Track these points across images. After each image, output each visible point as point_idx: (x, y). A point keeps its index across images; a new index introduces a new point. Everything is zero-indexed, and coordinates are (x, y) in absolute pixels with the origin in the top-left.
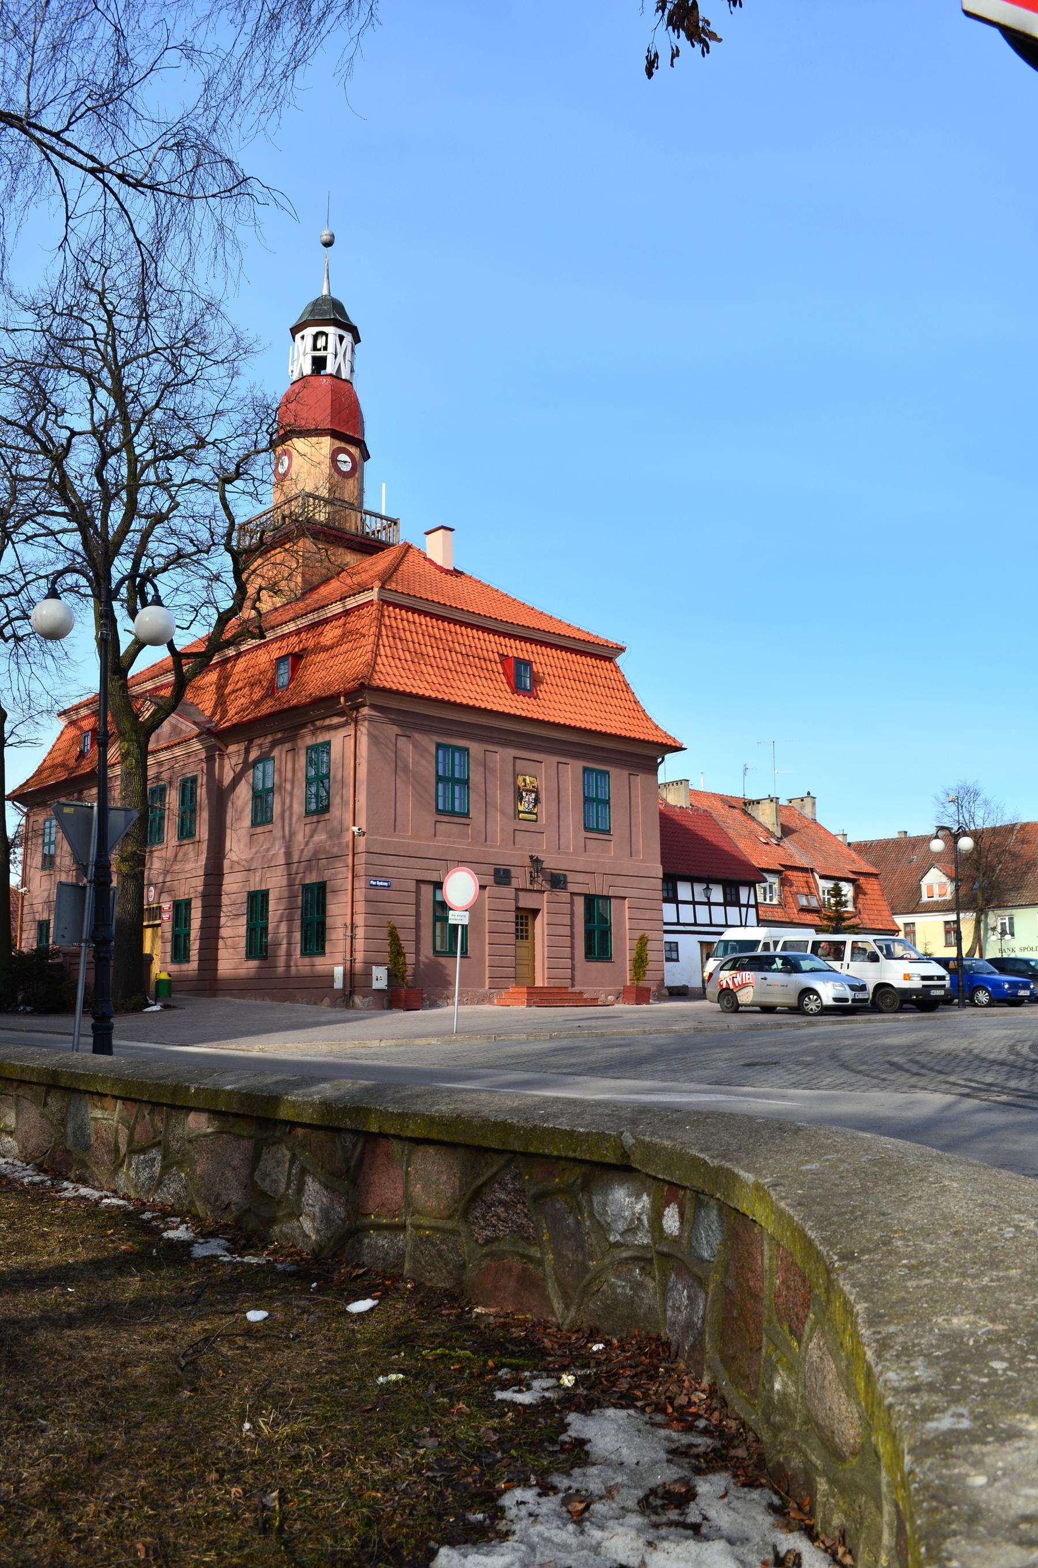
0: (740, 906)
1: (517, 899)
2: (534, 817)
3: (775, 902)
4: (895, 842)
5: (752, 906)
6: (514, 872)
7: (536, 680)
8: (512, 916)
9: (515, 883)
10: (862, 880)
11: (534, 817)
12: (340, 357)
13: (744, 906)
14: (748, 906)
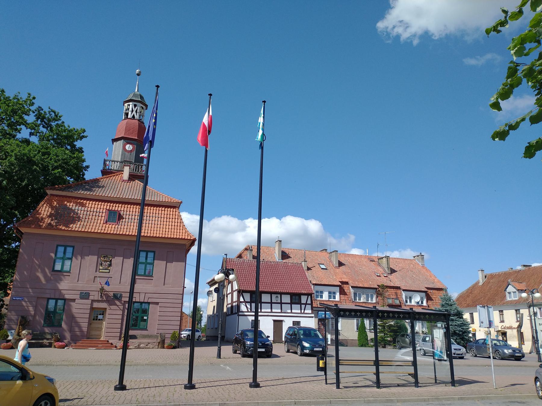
1: (92, 304)
6: (91, 293)
8: (88, 311)
9: (91, 298)
12: (134, 112)
14: (306, 304)
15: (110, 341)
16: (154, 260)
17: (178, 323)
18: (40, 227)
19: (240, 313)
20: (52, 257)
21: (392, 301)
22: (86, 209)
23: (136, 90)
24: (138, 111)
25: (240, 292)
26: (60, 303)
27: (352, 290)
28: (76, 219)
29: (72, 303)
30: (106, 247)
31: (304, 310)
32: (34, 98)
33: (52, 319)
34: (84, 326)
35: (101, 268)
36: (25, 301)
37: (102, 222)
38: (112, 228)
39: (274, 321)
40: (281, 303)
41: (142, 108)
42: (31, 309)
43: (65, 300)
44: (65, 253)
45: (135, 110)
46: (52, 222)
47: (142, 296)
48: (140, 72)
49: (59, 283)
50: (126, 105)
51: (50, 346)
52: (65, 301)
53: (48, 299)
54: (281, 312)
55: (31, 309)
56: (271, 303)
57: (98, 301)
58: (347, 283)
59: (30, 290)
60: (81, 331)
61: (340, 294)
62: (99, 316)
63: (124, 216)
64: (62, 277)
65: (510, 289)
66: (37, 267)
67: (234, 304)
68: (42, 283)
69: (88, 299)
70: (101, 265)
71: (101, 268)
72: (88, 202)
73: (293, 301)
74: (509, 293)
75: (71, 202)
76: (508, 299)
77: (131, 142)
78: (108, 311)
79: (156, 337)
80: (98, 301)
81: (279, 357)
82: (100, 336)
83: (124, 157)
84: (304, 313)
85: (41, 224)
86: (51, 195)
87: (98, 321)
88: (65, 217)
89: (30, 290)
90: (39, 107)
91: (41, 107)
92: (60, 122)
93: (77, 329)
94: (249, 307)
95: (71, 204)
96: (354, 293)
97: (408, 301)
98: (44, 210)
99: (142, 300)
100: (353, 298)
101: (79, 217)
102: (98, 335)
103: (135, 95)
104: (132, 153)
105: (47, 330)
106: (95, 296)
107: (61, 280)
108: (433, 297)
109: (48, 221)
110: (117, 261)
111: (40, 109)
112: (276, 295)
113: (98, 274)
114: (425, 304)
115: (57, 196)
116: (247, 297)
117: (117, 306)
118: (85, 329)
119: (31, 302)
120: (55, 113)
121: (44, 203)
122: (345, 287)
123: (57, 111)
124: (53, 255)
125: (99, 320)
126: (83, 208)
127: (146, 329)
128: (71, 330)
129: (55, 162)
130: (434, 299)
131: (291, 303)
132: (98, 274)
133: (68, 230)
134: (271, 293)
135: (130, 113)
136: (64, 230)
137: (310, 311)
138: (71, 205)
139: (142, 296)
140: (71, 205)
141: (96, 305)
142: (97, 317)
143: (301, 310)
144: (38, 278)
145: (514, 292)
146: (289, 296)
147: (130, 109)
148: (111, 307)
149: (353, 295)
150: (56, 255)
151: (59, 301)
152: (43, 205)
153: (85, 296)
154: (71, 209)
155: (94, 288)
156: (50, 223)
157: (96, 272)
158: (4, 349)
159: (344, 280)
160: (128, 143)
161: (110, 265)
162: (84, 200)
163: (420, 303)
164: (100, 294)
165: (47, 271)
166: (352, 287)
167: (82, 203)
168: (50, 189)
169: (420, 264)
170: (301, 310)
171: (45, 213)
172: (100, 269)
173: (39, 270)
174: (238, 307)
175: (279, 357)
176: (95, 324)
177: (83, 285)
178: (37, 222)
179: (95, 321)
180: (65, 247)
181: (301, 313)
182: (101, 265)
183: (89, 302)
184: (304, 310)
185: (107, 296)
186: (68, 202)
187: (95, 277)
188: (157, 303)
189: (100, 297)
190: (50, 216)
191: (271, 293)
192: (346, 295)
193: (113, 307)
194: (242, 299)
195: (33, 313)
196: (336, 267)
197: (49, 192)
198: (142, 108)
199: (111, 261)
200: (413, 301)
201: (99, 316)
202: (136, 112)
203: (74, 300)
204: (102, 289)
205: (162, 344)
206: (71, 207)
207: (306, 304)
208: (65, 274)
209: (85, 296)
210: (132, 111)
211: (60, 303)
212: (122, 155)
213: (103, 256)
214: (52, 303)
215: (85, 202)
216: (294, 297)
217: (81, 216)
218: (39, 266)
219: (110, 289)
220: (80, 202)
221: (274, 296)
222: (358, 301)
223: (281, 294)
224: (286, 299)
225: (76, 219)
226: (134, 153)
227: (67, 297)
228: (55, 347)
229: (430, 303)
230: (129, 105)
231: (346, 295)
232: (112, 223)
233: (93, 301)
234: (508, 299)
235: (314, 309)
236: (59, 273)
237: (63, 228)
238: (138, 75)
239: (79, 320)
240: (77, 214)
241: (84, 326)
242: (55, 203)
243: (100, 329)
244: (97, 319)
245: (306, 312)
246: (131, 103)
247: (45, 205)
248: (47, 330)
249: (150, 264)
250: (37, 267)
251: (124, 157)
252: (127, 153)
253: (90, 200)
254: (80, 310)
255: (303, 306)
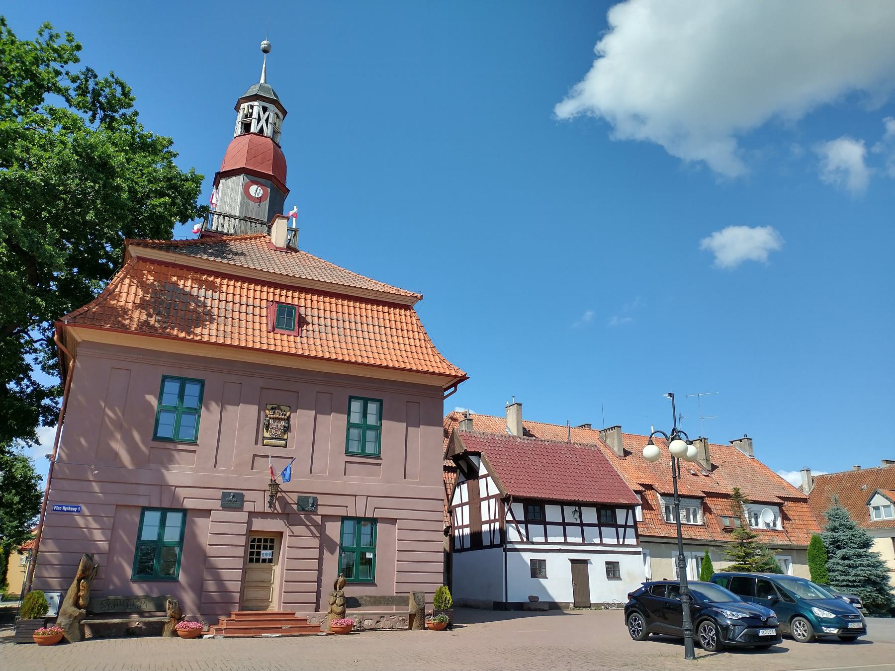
0: (617, 526)
1: (249, 523)
2: (283, 442)
3: (699, 522)
4: (850, 475)
5: (630, 527)
6: (248, 495)
7: (302, 322)
8: (242, 540)
9: (248, 507)
10: (708, 501)
11: (283, 442)
12: (263, 122)
13: (621, 526)
14: (625, 526)
15: (299, 615)
16: (380, 419)
17: (314, 575)
18: (125, 329)
19: (509, 546)
20: (149, 404)
21: (731, 522)
22: (223, 297)
23: (262, 81)
24: (270, 120)
25: (504, 500)
26: (174, 519)
27: (662, 501)
28: (203, 317)
29: (200, 521)
30: (284, 386)
31: (624, 538)
32: (78, 48)
33: (152, 561)
34: (232, 578)
35: (267, 435)
36: (84, 516)
37: (264, 328)
38: (285, 342)
39: (607, 563)
40: (582, 525)
41: (278, 116)
42: (98, 535)
43: (185, 512)
44: (181, 396)
45: (264, 117)
46: (152, 321)
47: (361, 502)
48: (269, 45)
49: (167, 469)
50: (245, 106)
51: (155, 630)
52: (185, 516)
53: (145, 509)
54: (583, 544)
55: (98, 535)
56: (564, 524)
57: (263, 515)
58: (649, 487)
59: (96, 487)
60: (223, 590)
61: (643, 509)
62: (263, 552)
63: (309, 319)
64: (175, 453)
65: (878, 500)
66: (112, 428)
67: (485, 528)
68: (125, 467)
69: (240, 509)
70: (267, 427)
71: (267, 435)
72: (225, 281)
73: (603, 520)
74: (877, 508)
75: (187, 279)
76: (874, 518)
77: (259, 180)
78: (286, 541)
79: (401, 601)
80: (263, 515)
81: (872, 643)
82: (267, 601)
83: (247, 210)
84: (624, 545)
85: (127, 322)
86: (140, 258)
87: (260, 565)
88: (176, 311)
89: (96, 487)
90: (88, 70)
91: (92, 71)
92: (129, 112)
93: (211, 586)
94: (523, 531)
95: (189, 283)
96: (667, 508)
97: (753, 520)
98: (126, 292)
99: (361, 514)
100: (664, 514)
101: (210, 313)
102: (262, 600)
103: (262, 87)
104: (263, 203)
105: (138, 590)
106: (257, 502)
107: (171, 460)
108: (790, 513)
109: (138, 316)
110: (301, 418)
111: (90, 73)
112: (573, 508)
113: (261, 450)
114: (779, 527)
115: (152, 262)
116: (519, 510)
117: (307, 526)
118: (234, 586)
119: (96, 517)
120: (123, 88)
121: (125, 277)
122: (649, 494)
123: (129, 85)
124: (153, 400)
125: (264, 561)
126: (217, 295)
127: (372, 583)
128: (199, 589)
129: (150, 182)
130: (791, 517)
131: (600, 525)
132: (261, 450)
133: (192, 341)
134: (562, 503)
135: (254, 123)
136: (184, 339)
137: (633, 541)
138: (187, 285)
139: (361, 502)
140: (187, 285)
141: (259, 525)
142: (259, 554)
143: (618, 538)
144: (116, 455)
145: (884, 507)
146: (594, 510)
147: (255, 115)
148: (293, 528)
149: (663, 510)
150: (160, 403)
151: (170, 515)
152: (123, 279)
153: (233, 501)
154: (190, 294)
155: (254, 482)
156: (146, 323)
157: (256, 443)
158: (41, 644)
159: (647, 482)
160: (254, 183)
161: (287, 429)
162: (217, 277)
163: (772, 525)
164: (268, 499)
165: (136, 436)
166: (663, 495)
167: (214, 282)
168: (138, 245)
169: (747, 454)
170: (618, 538)
171: (131, 298)
172: (264, 438)
173: (118, 436)
174: (503, 533)
175: (872, 643)
176: (257, 572)
177: (230, 476)
178: (114, 318)
179: (254, 565)
180: (183, 382)
181: (618, 545)
182: (267, 427)
183: (243, 516)
184: (624, 538)
185: (285, 504)
186: (180, 278)
187: (255, 456)
188: (393, 521)
189: (267, 505)
190: (143, 305)
191: (562, 503)
192: (653, 509)
193: (299, 530)
194: (509, 517)
195: (104, 545)
196: (620, 457)
197: (134, 251)
198: (278, 116)
199: (289, 418)
200: (760, 520)
201: (263, 552)
202: (267, 120)
203: (206, 513)
204: (274, 485)
205: (417, 620)
206: (188, 289)
207: (625, 526)
208: (180, 447)
209: (233, 501)
210: (259, 120)
211: (174, 519)
212: (242, 205)
213: (269, 407)
214: (152, 518)
215: (218, 280)
216: (603, 512)
217: (215, 311)
218: (119, 427)
219: (298, 484)
220: (206, 280)
221: (568, 510)
222: (692, 523)
223: (579, 504)
224: (590, 515)
225: (203, 317)
226: (266, 204)
227: (188, 504)
228: (175, 634)
229: (788, 524)
230: (252, 107)
231: (653, 509)
232: (283, 331)
233: (252, 515)
234: (874, 518)
235: (641, 539)
236: (170, 446)
237: (183, 335)
238: (265, 51)
239: (219, 562)
240: (205, 306)
241: (232, 578)
242: (151, 278)
243: (266, 585)
244: (258, 560)
245: (627, 542)
246: (256, 103)
247: (127, 281)
248: (138, 590)
249: (371, 428)
250: (112, 428)
251: (247, 210)
252: (252, 203)
253: (230, 277)
254: (220, 537)
255: (621, 530)
